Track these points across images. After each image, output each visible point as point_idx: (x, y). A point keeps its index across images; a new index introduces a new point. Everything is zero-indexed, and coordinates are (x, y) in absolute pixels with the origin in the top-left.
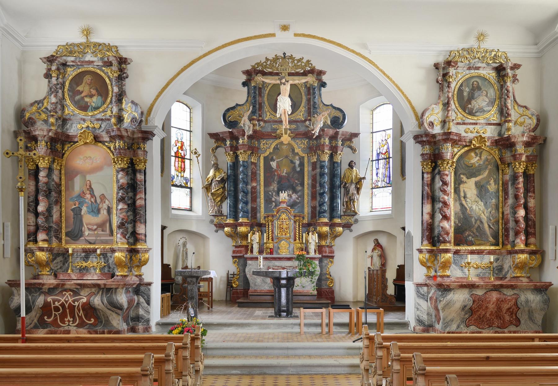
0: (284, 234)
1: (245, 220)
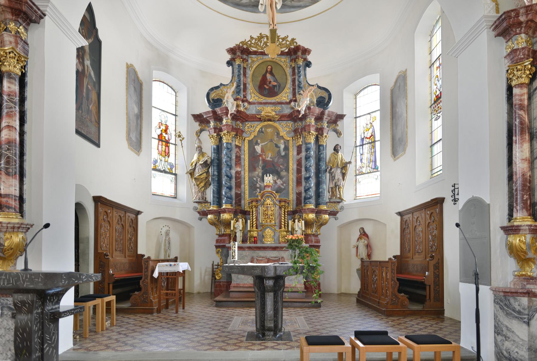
0: (269, 221)
1: (229, 206)
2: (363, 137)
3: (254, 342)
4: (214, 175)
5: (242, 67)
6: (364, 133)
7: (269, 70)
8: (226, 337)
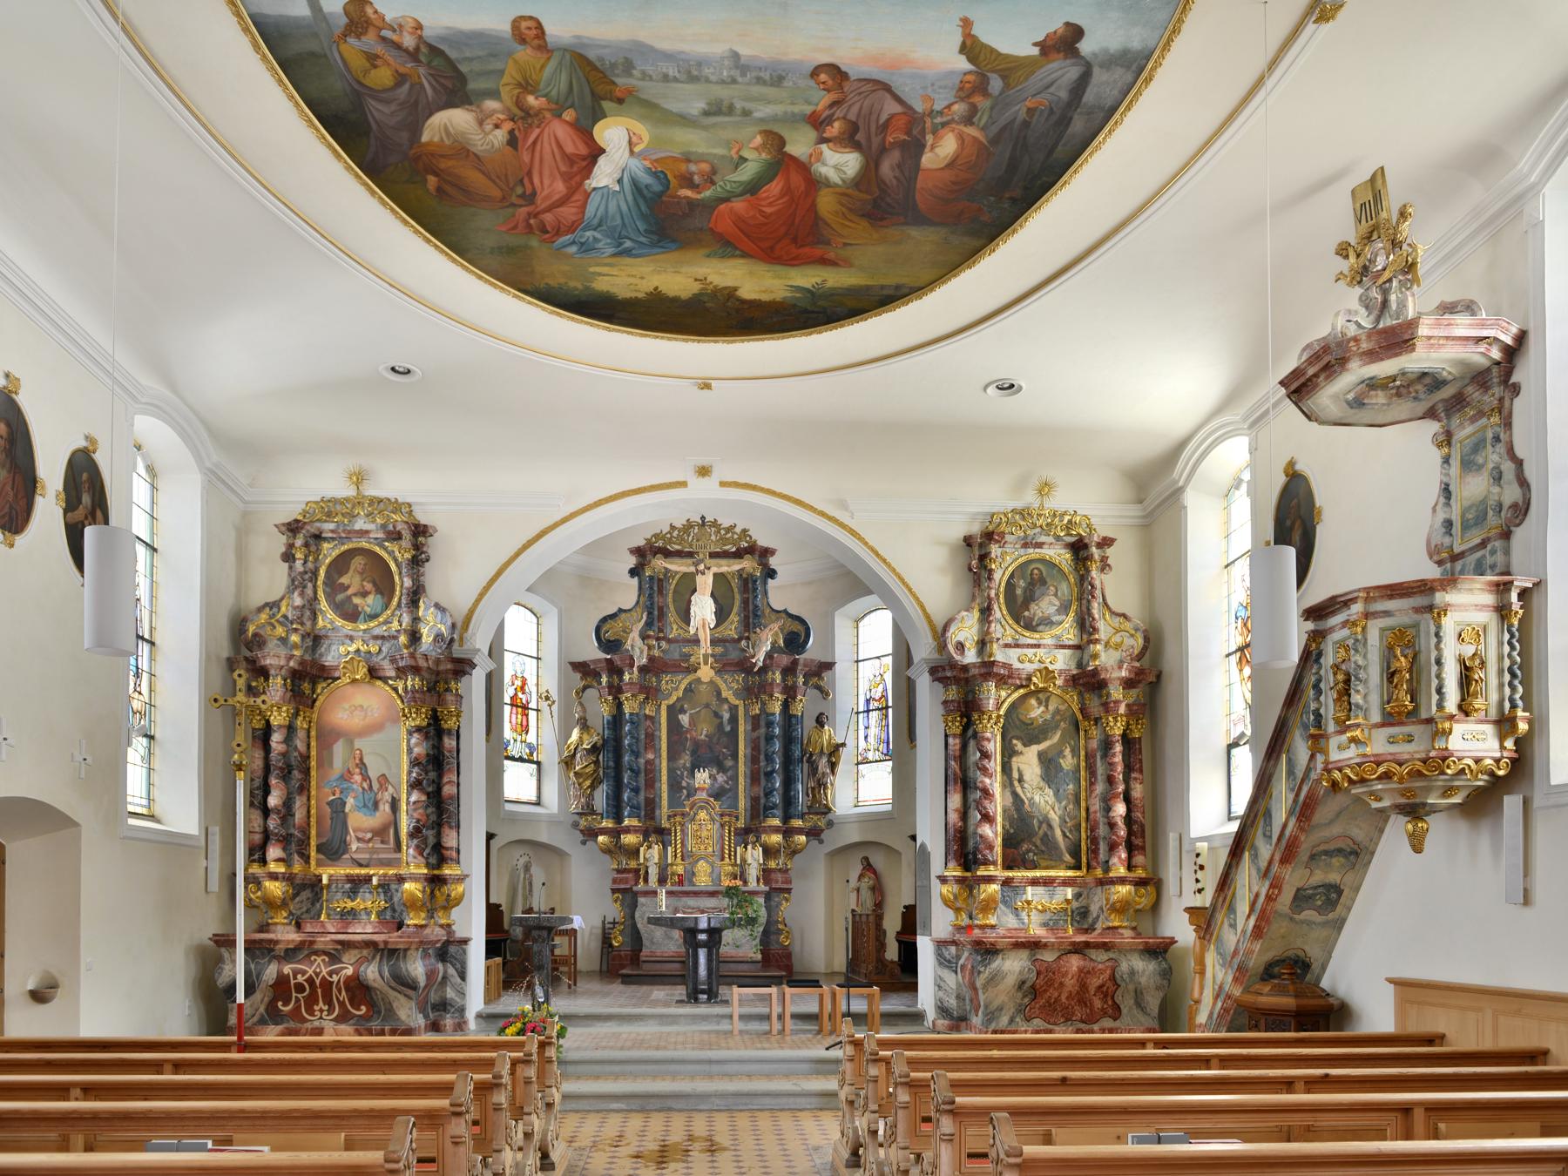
1: (635, 822)
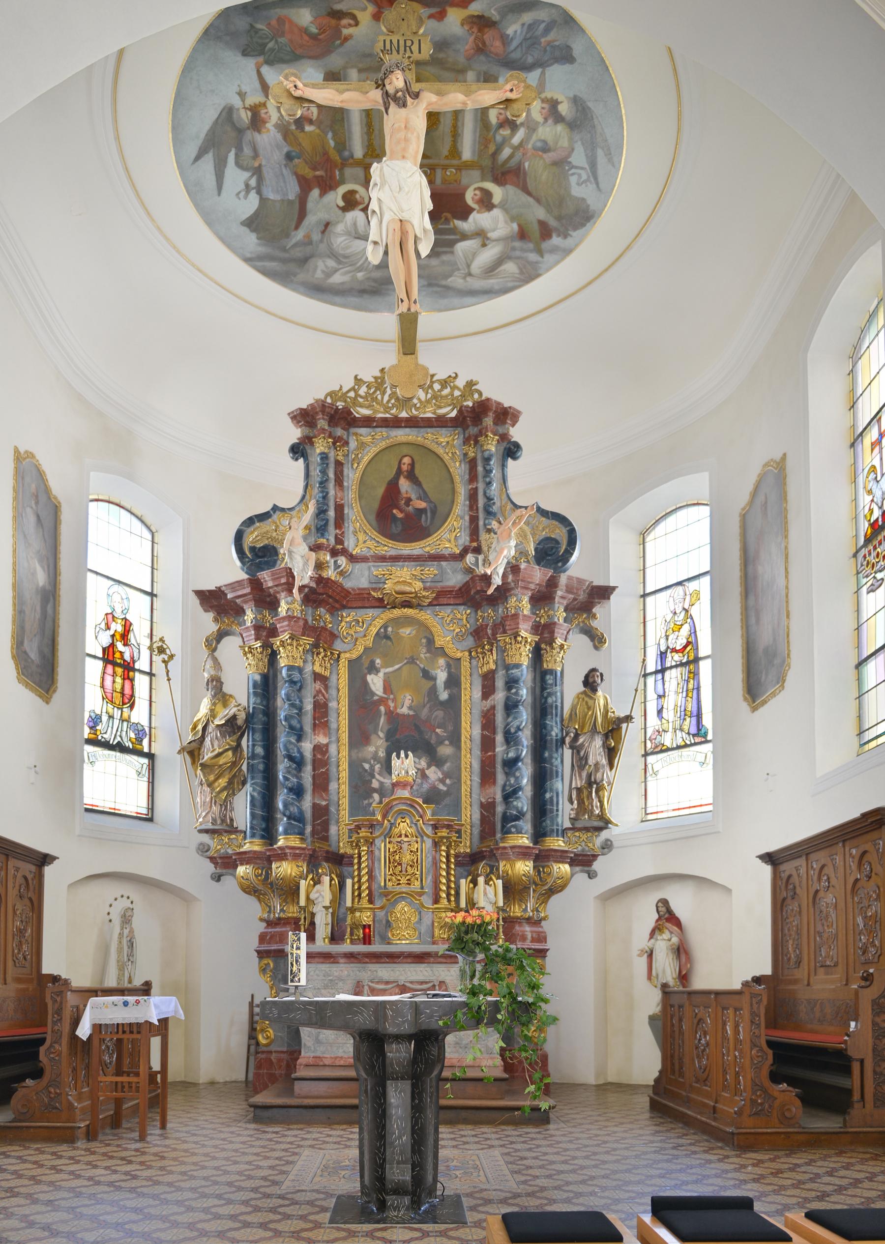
0: (403, 881)
1: (294, 841)
2: (663, 649)
3: (353, 1227)
4: (253, 756)
5: (332, 459)
6: (667, 637)
7: (405, 468)
8: (273, 1210)
